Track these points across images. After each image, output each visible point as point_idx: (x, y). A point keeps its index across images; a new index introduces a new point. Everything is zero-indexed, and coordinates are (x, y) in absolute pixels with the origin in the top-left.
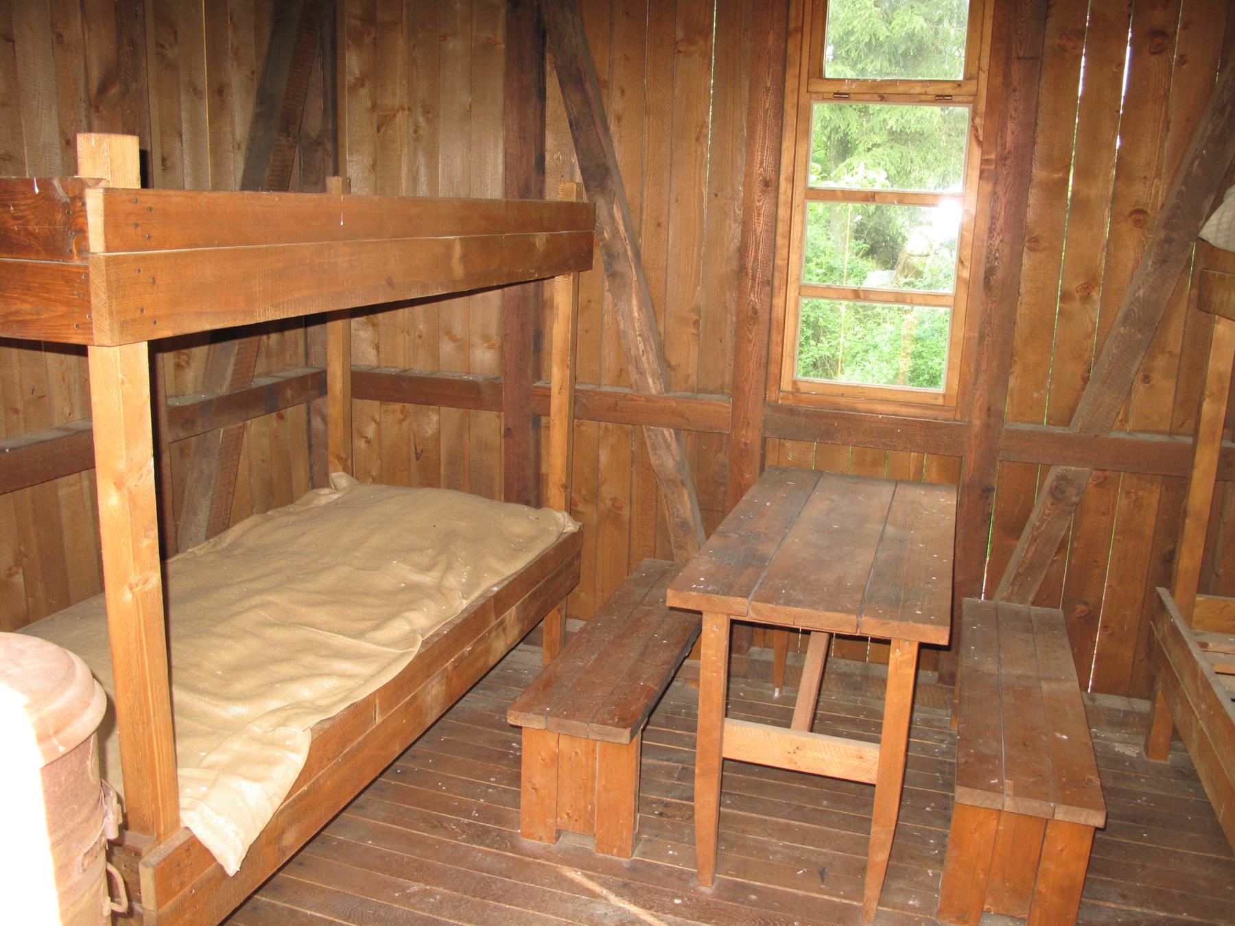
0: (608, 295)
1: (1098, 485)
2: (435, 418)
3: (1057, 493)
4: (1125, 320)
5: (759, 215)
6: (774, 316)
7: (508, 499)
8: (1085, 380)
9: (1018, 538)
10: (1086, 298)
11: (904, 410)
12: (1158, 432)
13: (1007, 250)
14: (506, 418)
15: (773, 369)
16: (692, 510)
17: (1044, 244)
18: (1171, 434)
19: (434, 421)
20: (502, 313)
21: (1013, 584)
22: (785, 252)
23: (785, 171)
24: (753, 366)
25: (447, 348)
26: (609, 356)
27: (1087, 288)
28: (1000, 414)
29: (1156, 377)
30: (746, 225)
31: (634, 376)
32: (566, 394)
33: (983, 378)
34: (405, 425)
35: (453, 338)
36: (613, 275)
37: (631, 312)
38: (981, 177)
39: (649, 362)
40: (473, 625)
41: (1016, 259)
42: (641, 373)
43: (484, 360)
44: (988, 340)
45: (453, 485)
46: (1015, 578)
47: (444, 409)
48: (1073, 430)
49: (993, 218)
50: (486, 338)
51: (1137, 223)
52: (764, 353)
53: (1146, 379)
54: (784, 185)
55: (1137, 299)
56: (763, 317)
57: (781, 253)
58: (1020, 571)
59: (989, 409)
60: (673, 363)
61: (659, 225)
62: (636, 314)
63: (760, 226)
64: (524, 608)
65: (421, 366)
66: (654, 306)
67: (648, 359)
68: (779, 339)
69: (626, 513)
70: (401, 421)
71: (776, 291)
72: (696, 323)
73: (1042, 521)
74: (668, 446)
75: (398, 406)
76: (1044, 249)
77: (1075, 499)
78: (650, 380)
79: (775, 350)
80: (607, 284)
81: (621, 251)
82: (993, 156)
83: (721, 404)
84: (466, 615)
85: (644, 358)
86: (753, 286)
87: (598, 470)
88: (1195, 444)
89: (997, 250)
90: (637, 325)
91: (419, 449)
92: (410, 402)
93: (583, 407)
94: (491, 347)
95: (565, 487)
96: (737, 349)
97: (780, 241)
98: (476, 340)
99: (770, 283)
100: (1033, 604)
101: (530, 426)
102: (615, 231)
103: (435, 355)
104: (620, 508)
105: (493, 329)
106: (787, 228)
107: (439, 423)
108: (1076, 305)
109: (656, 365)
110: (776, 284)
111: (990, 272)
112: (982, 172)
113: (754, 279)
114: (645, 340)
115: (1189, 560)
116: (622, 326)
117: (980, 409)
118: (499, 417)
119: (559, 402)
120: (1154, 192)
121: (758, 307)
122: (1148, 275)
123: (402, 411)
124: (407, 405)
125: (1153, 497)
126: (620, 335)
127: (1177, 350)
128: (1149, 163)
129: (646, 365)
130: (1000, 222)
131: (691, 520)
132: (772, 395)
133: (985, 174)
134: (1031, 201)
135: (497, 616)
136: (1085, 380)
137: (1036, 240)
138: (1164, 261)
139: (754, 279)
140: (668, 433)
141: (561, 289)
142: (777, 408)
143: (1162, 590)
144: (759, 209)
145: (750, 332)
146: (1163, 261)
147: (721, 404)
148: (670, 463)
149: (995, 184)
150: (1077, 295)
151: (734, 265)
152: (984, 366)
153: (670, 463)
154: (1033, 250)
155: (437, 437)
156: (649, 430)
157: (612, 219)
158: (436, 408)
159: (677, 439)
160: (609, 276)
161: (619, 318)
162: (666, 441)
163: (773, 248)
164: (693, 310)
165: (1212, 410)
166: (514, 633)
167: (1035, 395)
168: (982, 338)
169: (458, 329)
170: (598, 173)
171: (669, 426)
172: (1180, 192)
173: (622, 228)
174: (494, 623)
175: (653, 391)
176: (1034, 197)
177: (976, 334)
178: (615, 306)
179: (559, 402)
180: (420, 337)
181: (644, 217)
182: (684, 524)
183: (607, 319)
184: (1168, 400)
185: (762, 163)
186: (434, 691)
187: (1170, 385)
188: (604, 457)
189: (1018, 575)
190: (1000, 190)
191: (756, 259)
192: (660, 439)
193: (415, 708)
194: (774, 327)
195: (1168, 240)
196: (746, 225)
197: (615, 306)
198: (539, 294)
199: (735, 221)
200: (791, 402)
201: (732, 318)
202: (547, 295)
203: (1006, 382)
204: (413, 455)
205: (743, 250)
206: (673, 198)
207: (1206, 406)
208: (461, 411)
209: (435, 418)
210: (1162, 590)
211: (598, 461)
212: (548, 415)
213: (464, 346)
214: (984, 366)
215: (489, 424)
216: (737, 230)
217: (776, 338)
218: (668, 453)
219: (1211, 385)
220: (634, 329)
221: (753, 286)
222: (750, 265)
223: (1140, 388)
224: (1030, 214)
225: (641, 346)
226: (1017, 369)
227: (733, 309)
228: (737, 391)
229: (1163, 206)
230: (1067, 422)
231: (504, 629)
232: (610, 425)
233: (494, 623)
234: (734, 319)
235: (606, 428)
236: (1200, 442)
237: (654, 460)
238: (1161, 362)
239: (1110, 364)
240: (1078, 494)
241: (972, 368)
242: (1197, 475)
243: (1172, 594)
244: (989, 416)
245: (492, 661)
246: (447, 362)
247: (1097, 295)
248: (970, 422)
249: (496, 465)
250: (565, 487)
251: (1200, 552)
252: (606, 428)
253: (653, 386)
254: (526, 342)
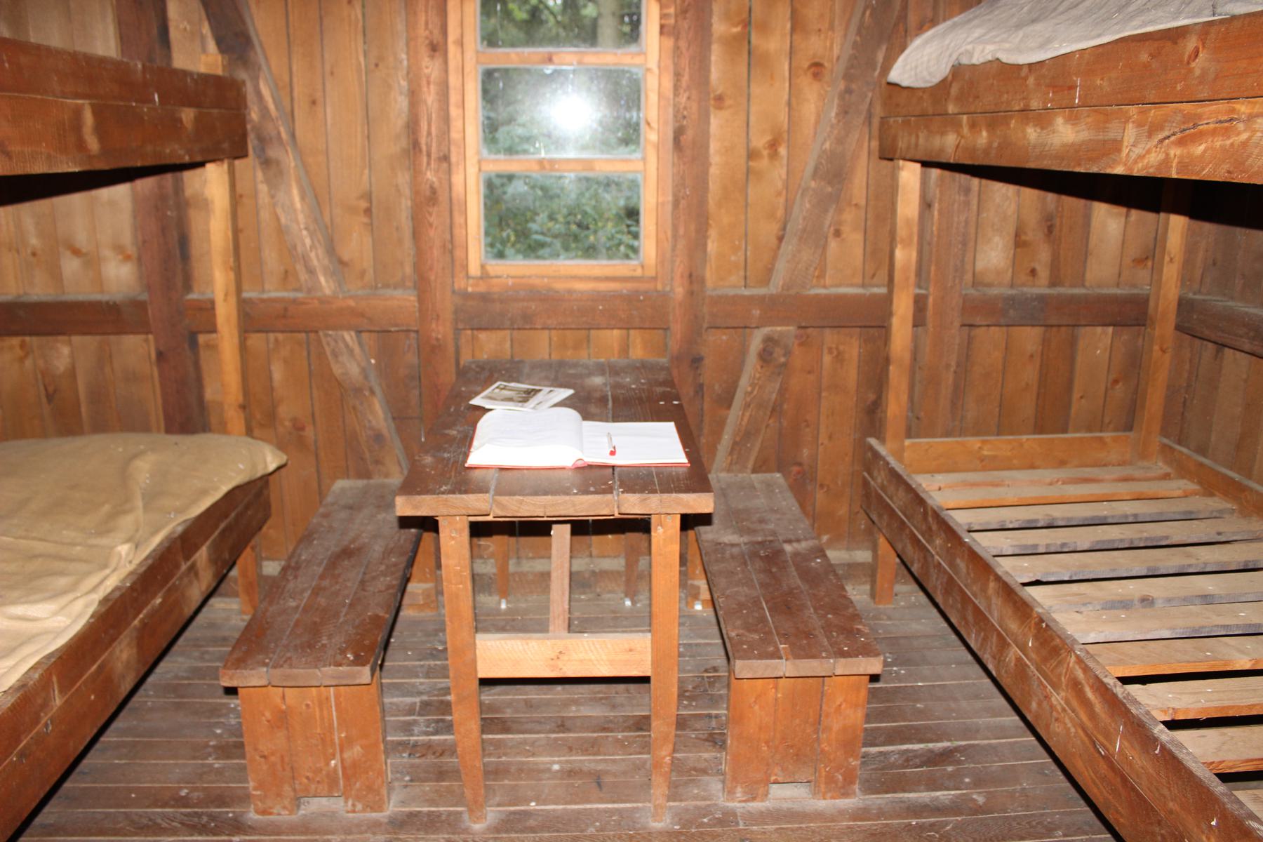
0: (263, 188)
1: (801, 344)
2: (66, 351)
3: (765, 356)
4: (815, 175)
5: (428, 83)
6: (454, 195)
7: (169, 431)
8: (781, 239)
9: (729, 407)
10: (774, 155)
11: (603, 287)
12: (852, 285)
13: (695, 107)
14: (156, 341)
15: (458, 253)
16: (386, 420)
17: (728, 102)
18: (863, 286)
19: (64, 354)
20: (135, 217)
21: (731, 453)
22: (460, 124)
23: (452, 35)
24: (436, 252)
25: (71, 266)
26: (271, 257)
27: (773, 145)
28: (702, 281)
29: (846, 229)
30: (414, 96)
31: (303, 276)
32: (233, 300)
33: (681, 244)
34: (28, 363)
35: (76, 252)
36: (266, 163)
37: (292, 204)
38: (661, 33)
39: (317, 258)
40: (158, 572)
41: (705, 118)
42: (311, 271)
43: (120, 278)
44: (683, 203)
45: (100, 426)
46: (733, 449)
47: (76, 339)
48: (775, 287)
49: (678, 76)
50: (119, 249)
51: (816, 76)
52: (448, 237)
53: (838, 233)
54: (452, 49)
55: (824, 152)
56: (443, 197)
57: (456, 124)
58: (738, 439)
59: (690, 276)
60: (346, 258)
61: (314, 102)
62: (298, 205)
63: (430, 97)
64: (216, 549)
65: (39, 290)
66: (317, 197)
67: (317, 255)
68: (462, 221)
69: (309, 432)
70: (22, 360)
71: (454, 169)
72: (368, 211)
73: (753, 385)
74: (351, 352)
75: (15, 341)
76: (730, 106)
77: (783, 360)
78: (322, 279)
79: (458, 232)
80: (260, 175)
81: (273, 133)
82: (672, 11)
83: (405, 299)
84: (150, 562)
85: (313, 255)
86: (429, 164)
87: (272, 389)
88: (891, 291)
89: (685, 108)
90: (301, 217)
91: (51, 389)
92: (31, 334)
93: (253, 320)
94: (128, 258)
95: (243, 407)
96: (416, 235)
97: (454, 112)
98: (107, 253)
99: (446, 158)
100: (754, 471)
101: (186, 346)
102: (264, 110)
103: (55, 274)
104: (303, 429)
105: (127, 238)
106: (460, 98)
107: (72, 355)
108: (763, 163)
109: (326, 262)
110: (453, 159)
111: (678, 133)
112: (662, 27)
113: (429, 155)
114: (312, 235)
115: (896, 405)
116: (283, 220)
117: (682, 276)
118: (147, 341)
119: (225, 313)
120: (833, 45)
121: (436, 185)
122: (832, 127)
123: (23, 345)
124: (27, 339)
125: (853, 349)
126: (281, 231)
127: (863, 203)
128: (822, 16)
129: (315, 262)
130: (685, 79)
131: (385, 432)
132: (460, 283)
133: (665, 30)
134: (713, 58)
135: (187, 558)
136: (781, 239)
137: (720, 99)
138: (846, 113)
139: (429, 155)
140: (349, 336)
141: (212, 182)
142: (466, 296)
143: (873, 441)
144: (428, 77)
145: (430, 214)
146: (844, 111)
147: (405, 299)
148: (354, 370)
149: (677, 39)
150: (765, 153)
151: (404, 142)
152: (681, 231)
153: (354, 370)
154: (720, 108)
155: (72, 373)
156: (326, 335)
157: (263, 96)
158: (66, 338)
159: (360, 344)
160: (261, 164)
161: (279, 211)
162: (347, 346)
163: (446, 119)
164: (362, 197)
165: (904, 256)
166: (206, 579)
167: (733, 258)
168: (676, 204)
169: (82, 238)
170: (235, 41)
171: (348, 328)
172: (855, 42)
173: (271, 106)
174: (184, 567)
175: (328, 292)
176: (716, 54)
177: (670, 198)
178: (273, 197)
179: (225, 313)
180: (34, 254)
181: (296, 94)
182: (379, 437)
183: (265, 215)
184: (859, 252)
185: (427, 24)
186: (125, 656)
187: (859, 237)
188: (278, 373)
189: (735, 444)
190: (683, 44)
191: (429, 133)
192: (341, 345)
193: (105, 680)
194: (456, 208)
195: (849, 91)
196: (414, 96)
197: (273, 197)
198: (179, 189)
199: (401, 93)
200: (482, 288)
201: (406, 203)
202: (189, 192)
203: (705, 245)
204: (44, 400)
205: (412, 126)
206: (328, 68)
207: (899, 254)
208: (98, 338)
209: (66, 351)
210: (873, 441)
211: (271, 379)
212: (213, 330)
213: (91, 261)
214: (681, 231)
215: (135, 350)
216: (402, 103)
217: (458, 219)
218: (351, 359)
219: (901, 232)
220: (298, 223)
221: (429, 164)
222: (423, 141)
223: (833, 244)
224: (715, 74)
225: (308, 241)
226: (713, 233)
227: (406, 191)
228: (422, 284)
229: (838, 58)
230: (766, 280)
231: (196, 574)
232: (280, 336)
233: (184, 567)
234: (409, 203)
235: (276, 340)
236: (896, 290)
237: (337, 370)
238: (848, 216)
239: (804, 218)
240: (785, 355)
241: (669, 234)
242: (895, 322)
243: (882, 440)
244: (691, 283)
245: (188, 612)
246: (75, 283)
247: (783, 151)
248: (672, 289)
249: (152, 397)
250: (243, 407)
251: (904, 398)
252: (276, 340)
253: (326, 285)
254: (170, 248)
